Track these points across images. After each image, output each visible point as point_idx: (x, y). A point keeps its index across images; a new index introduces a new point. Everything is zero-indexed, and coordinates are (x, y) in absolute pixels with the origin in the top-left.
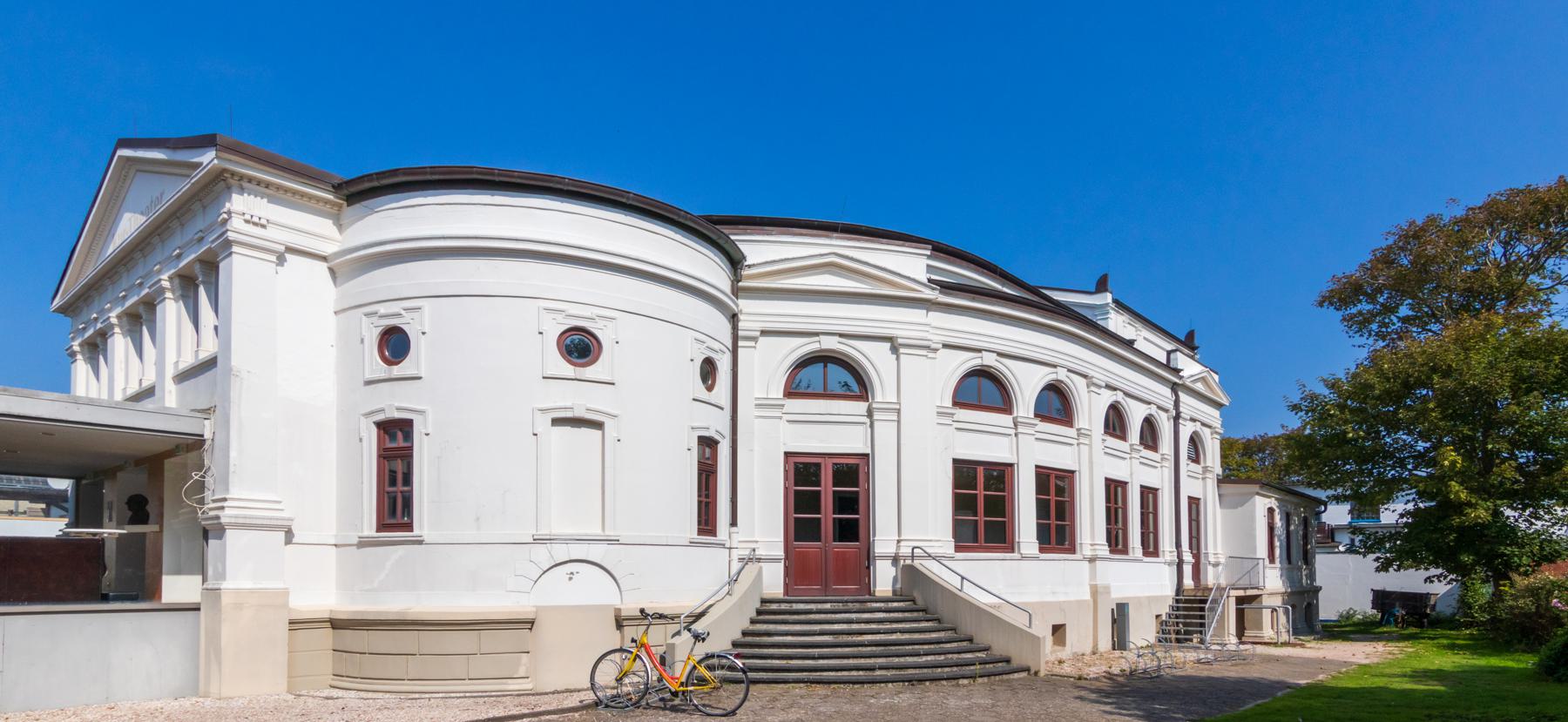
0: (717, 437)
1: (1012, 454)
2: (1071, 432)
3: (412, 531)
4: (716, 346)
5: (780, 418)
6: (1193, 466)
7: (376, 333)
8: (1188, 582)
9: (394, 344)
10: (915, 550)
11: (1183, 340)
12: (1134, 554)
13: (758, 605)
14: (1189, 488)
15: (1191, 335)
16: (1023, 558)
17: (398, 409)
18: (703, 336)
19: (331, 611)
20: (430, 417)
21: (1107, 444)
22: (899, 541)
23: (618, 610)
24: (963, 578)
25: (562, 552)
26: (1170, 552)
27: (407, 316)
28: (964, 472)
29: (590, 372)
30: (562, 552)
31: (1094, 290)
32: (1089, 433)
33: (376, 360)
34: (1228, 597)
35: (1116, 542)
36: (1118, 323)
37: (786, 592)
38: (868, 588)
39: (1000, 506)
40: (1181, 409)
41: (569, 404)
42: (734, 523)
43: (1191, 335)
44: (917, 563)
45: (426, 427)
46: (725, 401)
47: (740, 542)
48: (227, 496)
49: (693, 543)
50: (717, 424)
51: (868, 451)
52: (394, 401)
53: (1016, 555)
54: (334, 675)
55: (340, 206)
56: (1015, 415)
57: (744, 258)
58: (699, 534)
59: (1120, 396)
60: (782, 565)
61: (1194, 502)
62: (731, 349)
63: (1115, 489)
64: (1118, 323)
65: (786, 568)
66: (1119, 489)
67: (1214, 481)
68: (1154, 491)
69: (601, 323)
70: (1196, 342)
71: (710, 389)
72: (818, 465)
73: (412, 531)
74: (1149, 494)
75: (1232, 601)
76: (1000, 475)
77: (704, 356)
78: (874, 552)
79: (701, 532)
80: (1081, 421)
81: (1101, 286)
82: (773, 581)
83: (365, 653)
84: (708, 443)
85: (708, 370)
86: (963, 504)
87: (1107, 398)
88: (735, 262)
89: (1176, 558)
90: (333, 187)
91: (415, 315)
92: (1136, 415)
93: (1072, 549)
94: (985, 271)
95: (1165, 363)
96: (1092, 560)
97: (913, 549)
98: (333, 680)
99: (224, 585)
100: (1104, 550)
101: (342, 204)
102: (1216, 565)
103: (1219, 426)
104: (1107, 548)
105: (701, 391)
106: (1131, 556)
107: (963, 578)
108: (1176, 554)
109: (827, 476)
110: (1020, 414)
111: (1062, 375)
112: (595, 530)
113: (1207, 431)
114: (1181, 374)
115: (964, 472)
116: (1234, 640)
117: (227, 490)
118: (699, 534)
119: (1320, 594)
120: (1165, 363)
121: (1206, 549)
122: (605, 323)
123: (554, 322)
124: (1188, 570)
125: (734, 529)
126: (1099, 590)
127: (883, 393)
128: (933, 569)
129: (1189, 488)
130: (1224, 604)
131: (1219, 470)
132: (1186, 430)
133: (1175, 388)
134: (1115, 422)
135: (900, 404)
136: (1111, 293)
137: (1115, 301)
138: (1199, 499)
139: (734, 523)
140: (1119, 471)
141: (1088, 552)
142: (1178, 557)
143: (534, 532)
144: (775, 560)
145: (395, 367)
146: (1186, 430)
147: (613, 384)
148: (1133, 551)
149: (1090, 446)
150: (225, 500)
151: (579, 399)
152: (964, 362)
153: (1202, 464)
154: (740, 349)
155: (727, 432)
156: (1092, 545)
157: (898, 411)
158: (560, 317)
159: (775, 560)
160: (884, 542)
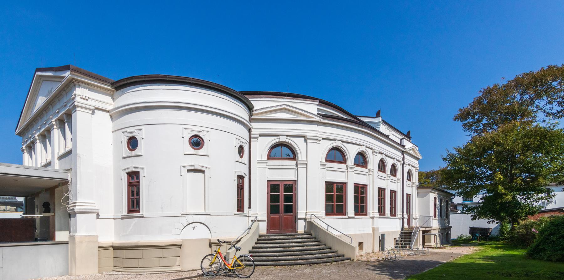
0: (244, 175)
1: (346, 179)
2: (366, 170)
4: (244, 141)
5: (266, 167)
6: (409, 182)
7: (127, 139)
8: (406, 226)
9: (133, 143)
10: (312, 216)
11: (406, 134)
12: (387, 215)
13: (258, 237)
14: (407, 190)
15: (409, 133)
16: (349, 218)
17: (134, 167)
18: (239, 137)
21: (379, 174)
22: (306, 213)
23: (210, 240)
24: (328, 226)
25: (191, 219)
26: (400, 214)
27: (137, 132)
28: (329, 186)
29: (200, 152)
30: (191, 219)
31: (375, 117)
32: (373, 170)
33: (127, 149)
34: (420, 231)
35: (381, 211)
36: (383, 129)
37: (267, 233)
38: (295, 230)
39: (341, 199)
40: (405, 161)
41: (193, 164)
42: (250, 207)
43: (409, 133)
44: (312, 220)
45: (144, 174)
46: (247, 162)
47: (252, 214)
48: (77, 202)
49: (236, 215)
50: (244, 171)
51: (296, 179)
52: (133, 165)
53: (346, 217)
55: (113, 91)
56: (347, 164)
57: (253, 107)
58: (237, 212)
59: (384, 156)
60: (265, 223)
61: (409, 195)
62: (249, 142)
63: (381, 191)
64: (383, 129)
65: (267, 223)
66: (383, 191)
67: (415, 188)
68: (395, 192)
69: (204, 133)
70: (411, 136)
71: (241, 157)
72: (279, 185)
74: (393, 192)
75: (421, 232)
76: (341, 187)
77: (240, 145)
78: (298, 217)
79: (238, 211)
80: (370, 166)
81: (378, 115)
82: (263, 228)
83: (124, 258)
84: (241, 177)
85: (241, 150)
86: (328, 198)
87: (379, 157)
88: (250, 109)
89: (402, 217)
90: (111, 84)
91: (140, 132)
92: (389, 163)
93: (366, 214)
94: (338, 110)
95: (400, 143)
96: (373, 218)
97: (311, 216)
98: (114, 268)
99: (76, 234)
100: (377, 214)
101: (114, 91)
102: (416, 219)
103: (418, 167)
104: (378, 213)
105: (239, 159)
106: (386, 216)
107: (328, 226)
108: (402, 215)
109: (282, 189)
110: (349, 164)
111: (364, 149)
112: (202, 211)
113: (414, 169)
114: (405, 147)
115: (329, 186)
116: (421, 246)
117: (77, 199)
118: (237, 212)
119: (451, 229)
120: (400, 143)
121: (412, 213)
122: (206, 133)
124: (406, 221)
125: (250, 209)
126: (375, 229)
127: (301, 157)
128: (318, 222)
129: (407, 190)
130: (418, 233)
131: (417, 184)
132: (407, 169)
133: (403, 153)
134: (382, 166)
135: (307, 161)
136: (381, 117)
137: (383, 120)
138: (410, 195)
139: (250, 207)
140: (383, 185)
141: (371, 215)
142: (403, 216)
143: (181, 212)
144: (263, 221)
145: (133, 152)
146: (407, 169)
148: (369, 213)
149: (373, 175)
150: (76, 203)
151: (197, 162)
152: (330, 145)
153: (412, 182)
154: (252, 142)
155: (247, 173)
156: (373, 212)
157: (307, 164)
158: (190, 131)
159: (263, 221)
160: (301, 214)
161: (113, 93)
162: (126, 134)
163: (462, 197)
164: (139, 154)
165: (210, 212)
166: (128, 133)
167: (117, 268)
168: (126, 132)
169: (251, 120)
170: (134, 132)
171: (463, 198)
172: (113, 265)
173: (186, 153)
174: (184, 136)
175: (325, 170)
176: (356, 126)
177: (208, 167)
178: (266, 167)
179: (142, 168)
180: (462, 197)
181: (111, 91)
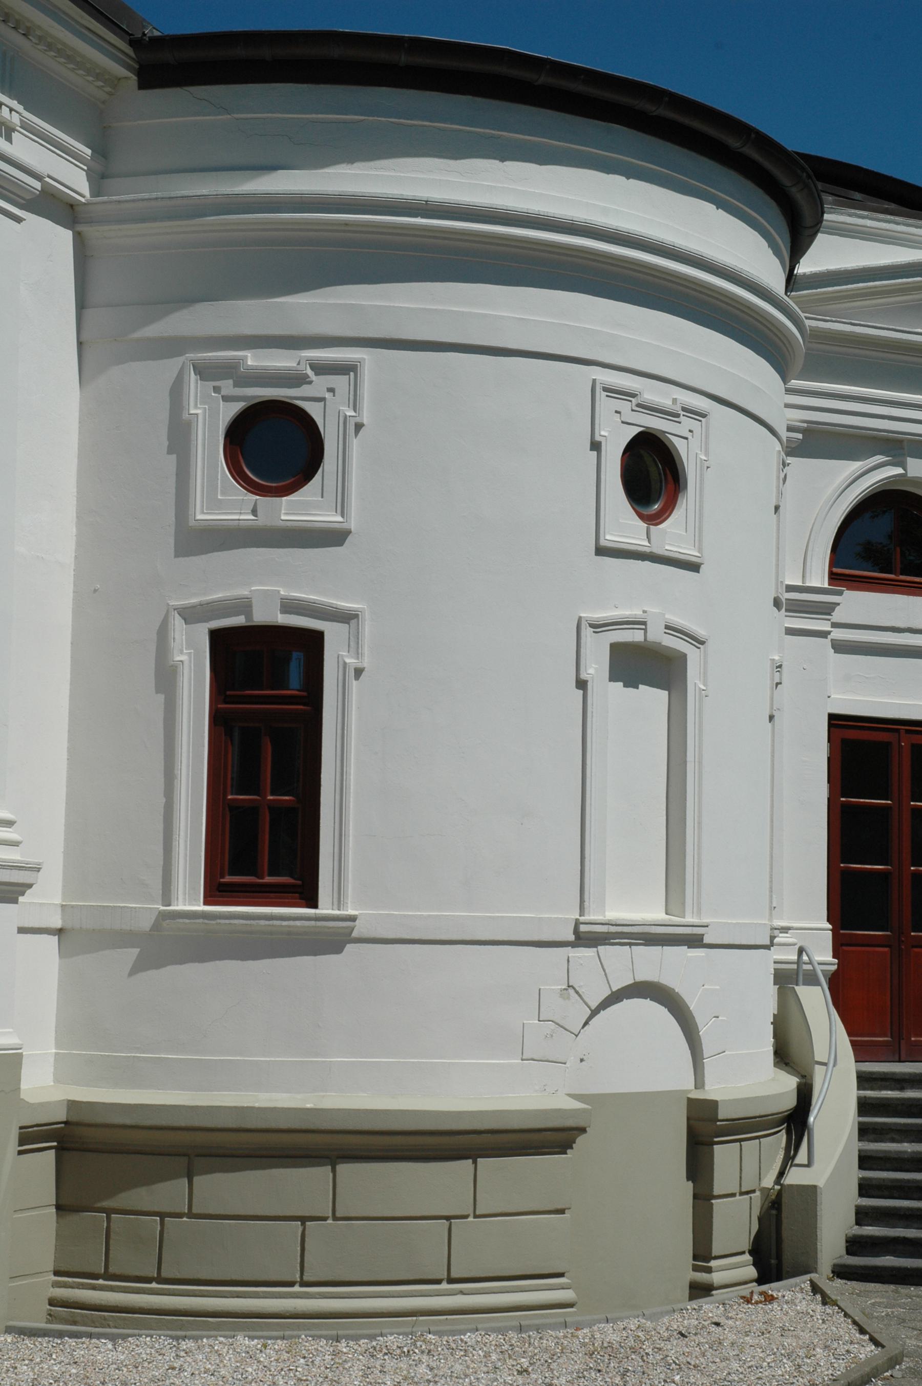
3: (315, 906)
5: (824, 634)
7: (228, 412)
19: (72, 1105)
20: (367, 628)
27: (319, 385)
45: (358, 655)
54: (57, 1273)
55: (115, 82)
73: (315, 906)
91: (340, 382)
98: (56, 1285)
123: (617, 417)
147: (694, 567)
161: (110, 94)
162: (625, 406)
163: (778, 986)
164: (329, 518)
165: (705, 921)
166: (638, 405)
167: (94, 1288)
168: (634, 396)
169: (791, 281)
170: (299, 380)
171: (778, 988)
172: (51, 1267)
173: (611, 538)
174: (603, 432)
175: (827, 642)
176: (411, 221)
177: (700, 631)
178: (824, 634)
179: (347, 617)
180: (778, 986)
181: (100, 75)
